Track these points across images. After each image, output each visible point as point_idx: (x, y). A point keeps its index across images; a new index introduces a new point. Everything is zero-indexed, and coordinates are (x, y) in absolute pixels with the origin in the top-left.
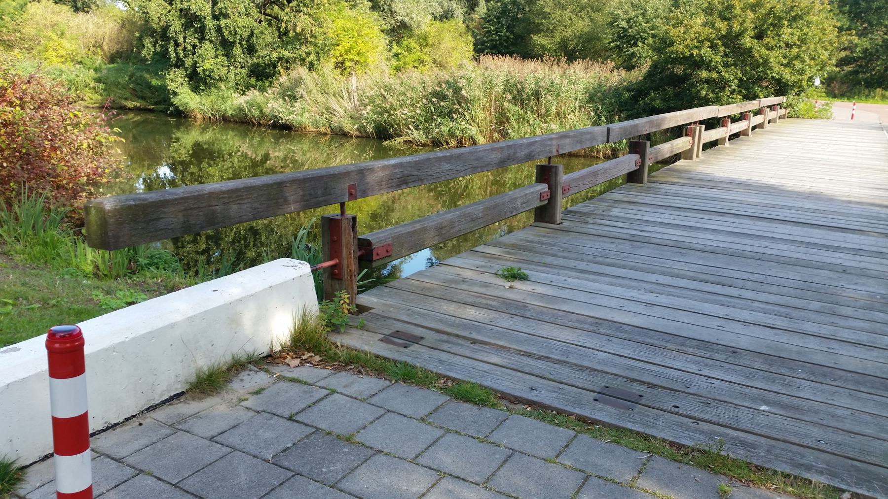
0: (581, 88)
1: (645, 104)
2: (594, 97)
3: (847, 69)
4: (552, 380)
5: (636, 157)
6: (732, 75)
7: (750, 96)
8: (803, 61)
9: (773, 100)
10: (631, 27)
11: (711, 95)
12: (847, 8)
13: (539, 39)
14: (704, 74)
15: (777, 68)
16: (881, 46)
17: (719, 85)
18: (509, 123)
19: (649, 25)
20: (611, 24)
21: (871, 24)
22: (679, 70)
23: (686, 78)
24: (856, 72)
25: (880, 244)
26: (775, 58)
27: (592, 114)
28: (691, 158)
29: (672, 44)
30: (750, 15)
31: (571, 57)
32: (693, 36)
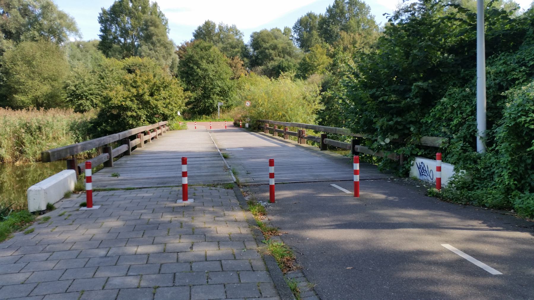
0: (65, 123)
1: (102, 129)
2: (73, 128)
3: (190, 107)
5: (107, 154)
6: (143, 113)
7: (153, 122)
8: (172, 105)
9: (162, 123)
10: (77, 90)
11: (134, 123)
12: (184, 79)
13: (19, 97)
14: (129, 113)
15: (162, 109)
17: (137, 118)
18: (25, 146)
19: (87, 88)
20: (65, 88)
21: (196, 87)
22: (115, 112)
23: (118, 116)
24: (193, 108)
26: (160, 104)
27: (74, 136)
28: (141, 147)
29: (111, 99)
30: (146, 86)
31: (48, 107)
32: (121, 96)
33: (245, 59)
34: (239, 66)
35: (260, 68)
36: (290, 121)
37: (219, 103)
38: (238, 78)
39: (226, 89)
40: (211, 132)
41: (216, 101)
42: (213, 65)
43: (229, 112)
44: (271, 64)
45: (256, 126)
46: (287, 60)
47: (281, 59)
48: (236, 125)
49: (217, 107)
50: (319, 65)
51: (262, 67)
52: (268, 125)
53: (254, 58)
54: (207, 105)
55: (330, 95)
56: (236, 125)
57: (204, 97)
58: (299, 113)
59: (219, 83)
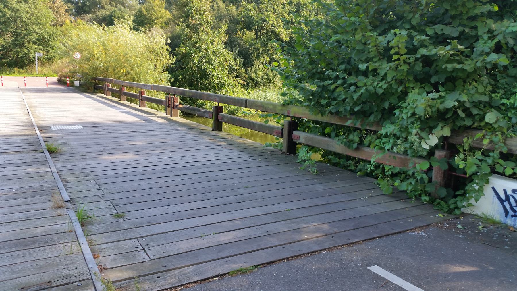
4: (354, 243)
16: (11, 43)
25: (16, 158)
33: (69, 5)
34: (62, 11)
35: (88, 16)
36: (138, 81)
37: (37, 54)
38: (61, 25)
39: (47, 37)
40: (24, 91)
41: (32, 51)
42: (26, 6)
43: (50, 65)
44: (101, 13)
45: (92, 84)
46: (120, 10)
47: (113, 8)
48: (61, 82)
49: (34, 58)
50: (157, 19)
51: (91, 15)
52: (110, 84)
53: (80, 5)
54: (20, 55)
55: (184, 51)
56: (61, 82)
57: (16, 45)
58: (149, 71)
59: (36, 28)
